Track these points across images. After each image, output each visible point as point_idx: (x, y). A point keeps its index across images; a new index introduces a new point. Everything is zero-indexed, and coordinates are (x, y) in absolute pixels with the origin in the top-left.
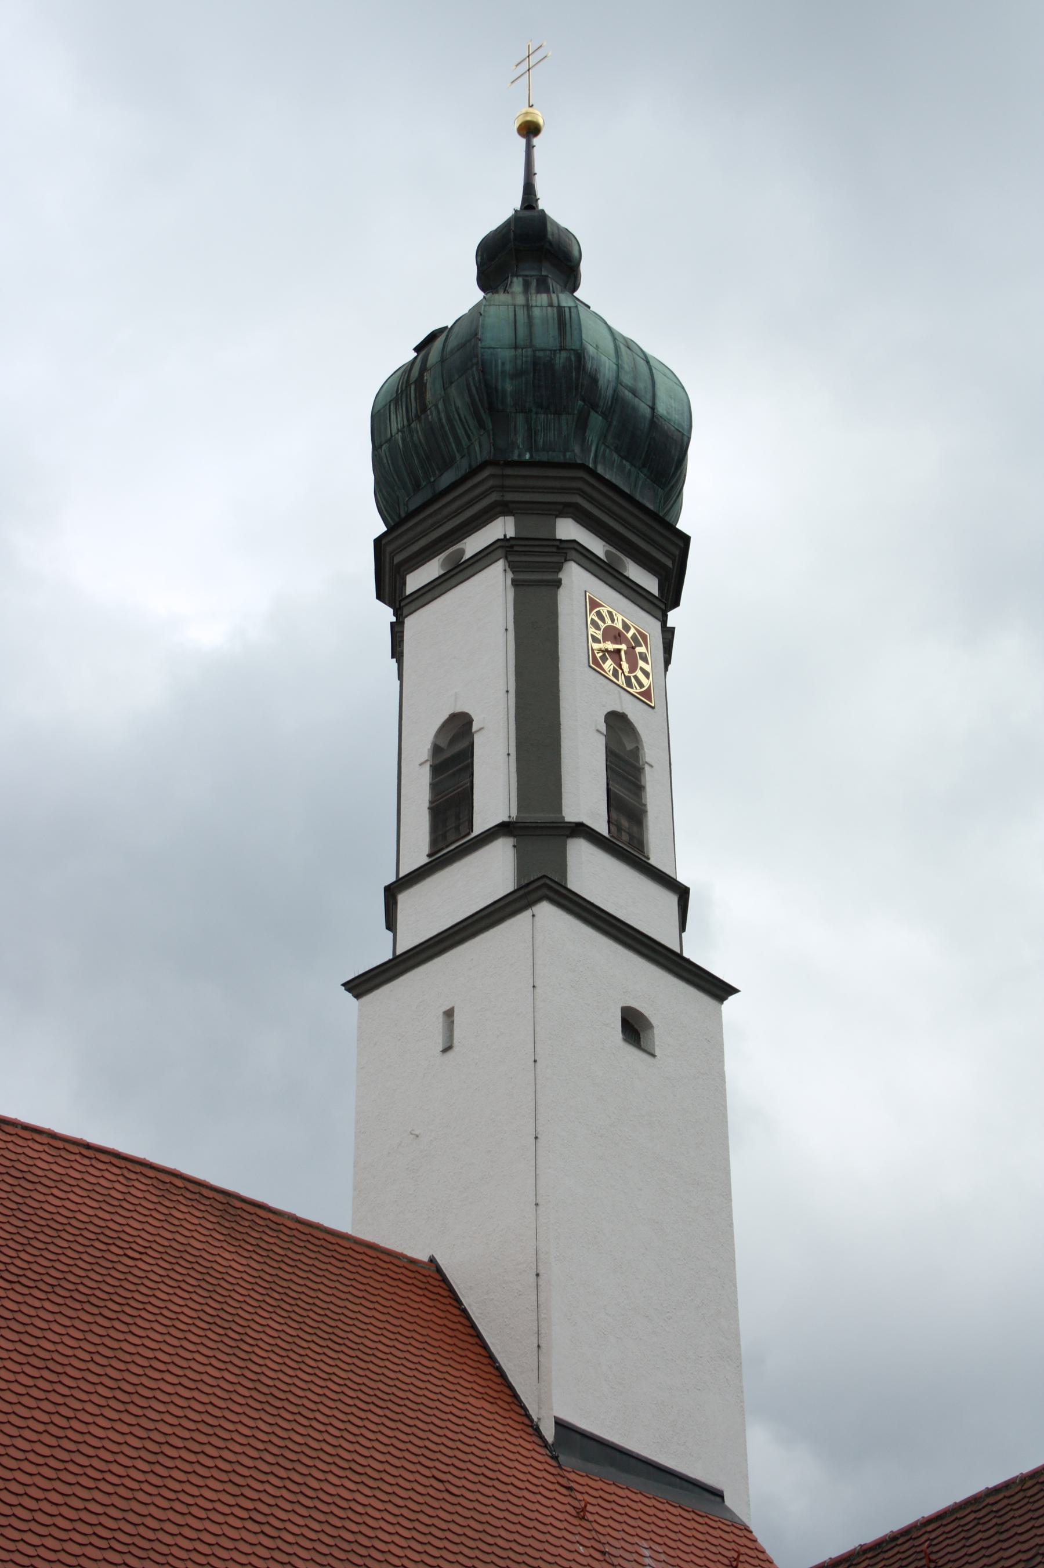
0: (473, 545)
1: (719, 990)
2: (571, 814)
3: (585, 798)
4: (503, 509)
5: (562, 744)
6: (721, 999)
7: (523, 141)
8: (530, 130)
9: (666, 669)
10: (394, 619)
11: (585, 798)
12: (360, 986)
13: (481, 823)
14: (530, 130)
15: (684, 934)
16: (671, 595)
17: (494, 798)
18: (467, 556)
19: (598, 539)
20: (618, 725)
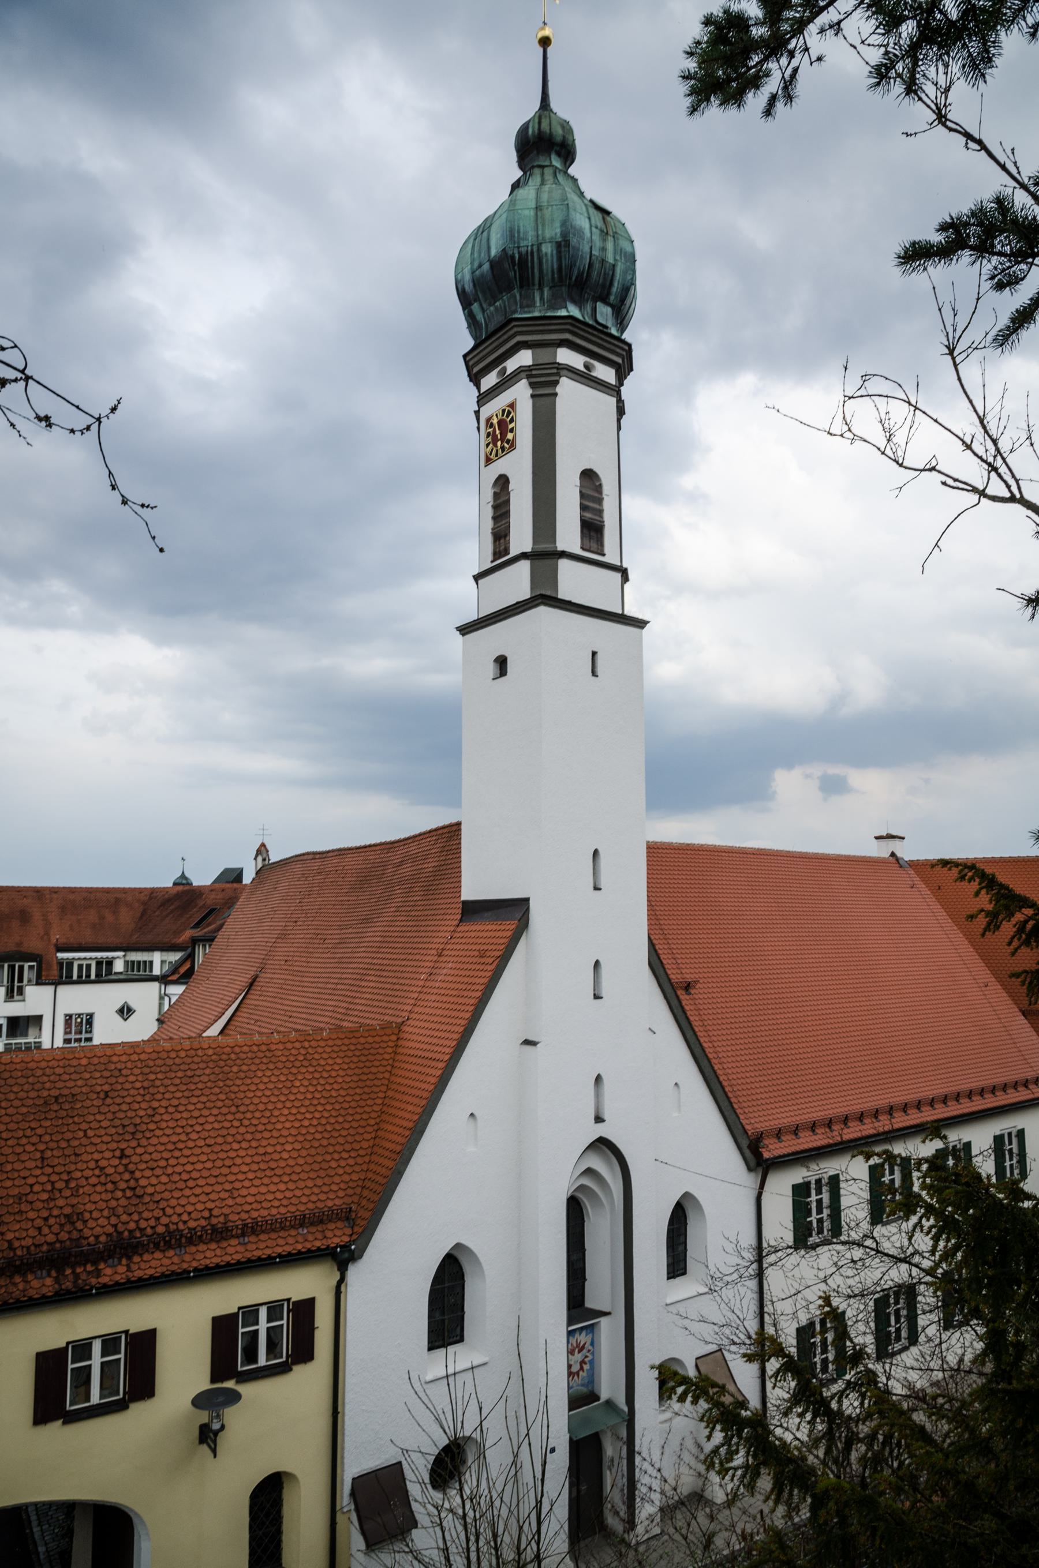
0: (512, 365)
1: (640, 624)
2: (561, 546)
3: (568, 535)
4: (526, 345)
5: (394, 1198)
6: (643, 628)
7: (541, 50)
8: (545, 42)
9: (619, 428)
10: (131, 1332)
11: (568, 535)
12: (465, 630)
13: (514, 552)
14: (545, 42)
15: (626, 586)
16: (624, 368)
17: (521, 539)
18: (508, 372)
19: (286, 1511)
20: (589, 476)
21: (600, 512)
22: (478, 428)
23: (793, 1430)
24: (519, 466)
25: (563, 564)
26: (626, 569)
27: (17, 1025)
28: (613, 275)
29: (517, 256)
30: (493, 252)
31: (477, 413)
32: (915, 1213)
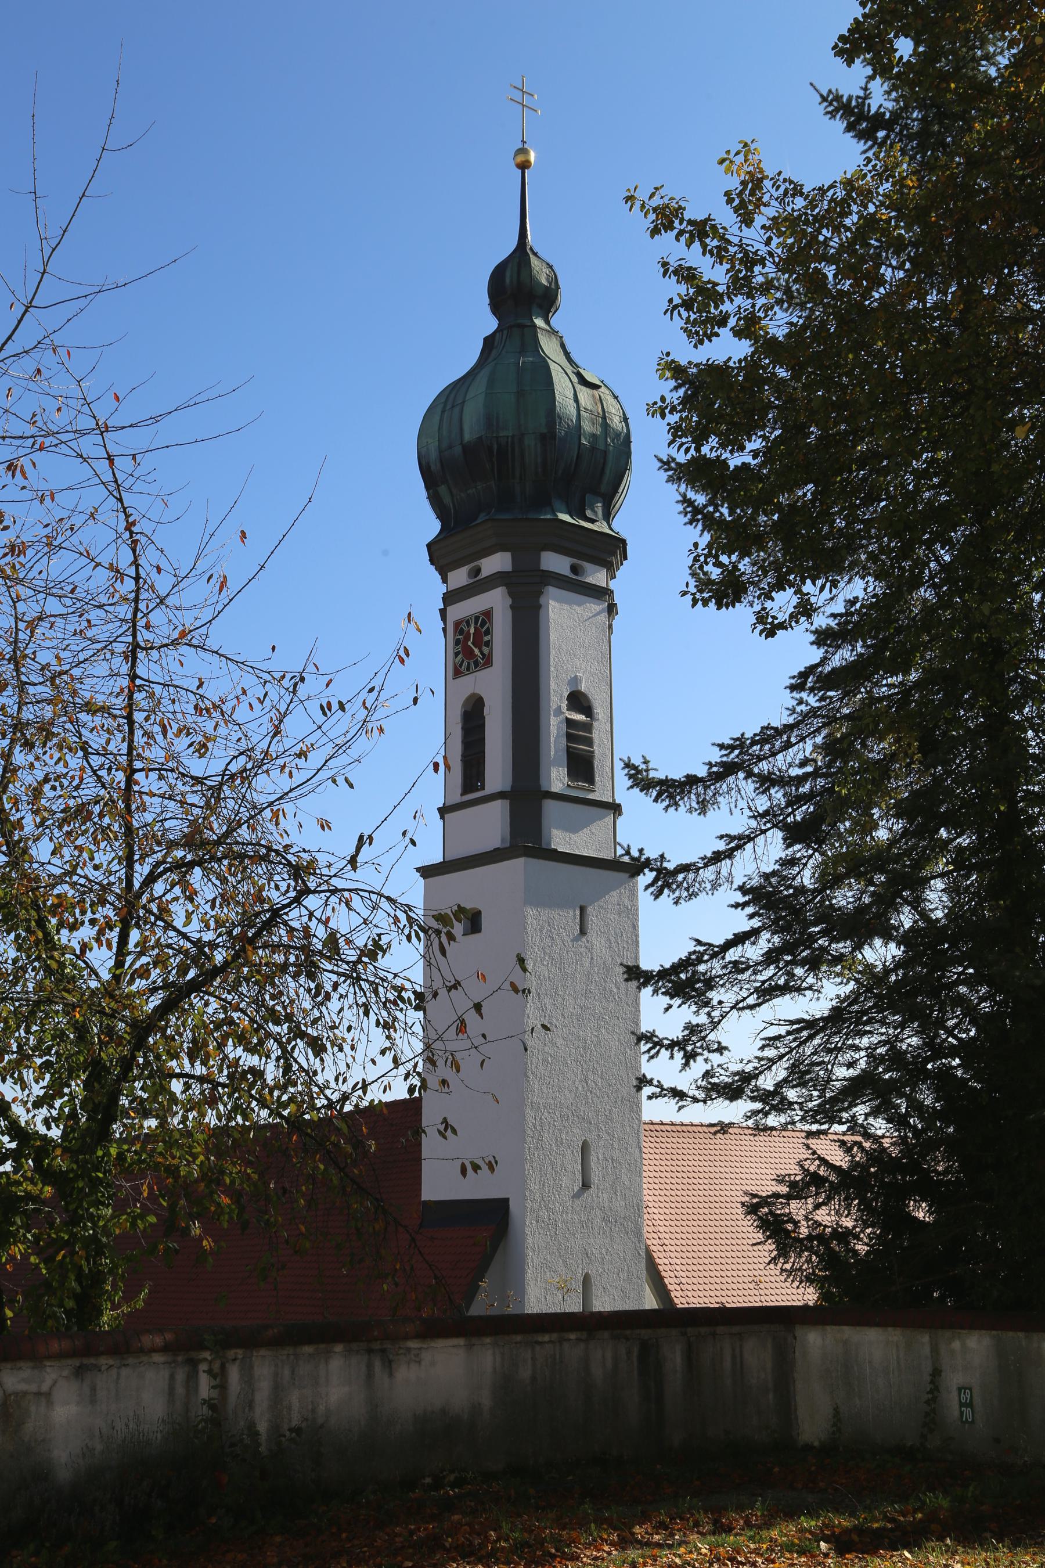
17: (497, 773)
20: (578, 701)
21: (589, 742)
22: (444, 630)
23: (881, 98)
24: (494, 684)
25: (549, 805)
26: (619, 806)
27: (911, 1565)
28: (605, 463)
29: (495, 446)
30: (467, 437)
31: (443, 613)
32: (853, 1514)
